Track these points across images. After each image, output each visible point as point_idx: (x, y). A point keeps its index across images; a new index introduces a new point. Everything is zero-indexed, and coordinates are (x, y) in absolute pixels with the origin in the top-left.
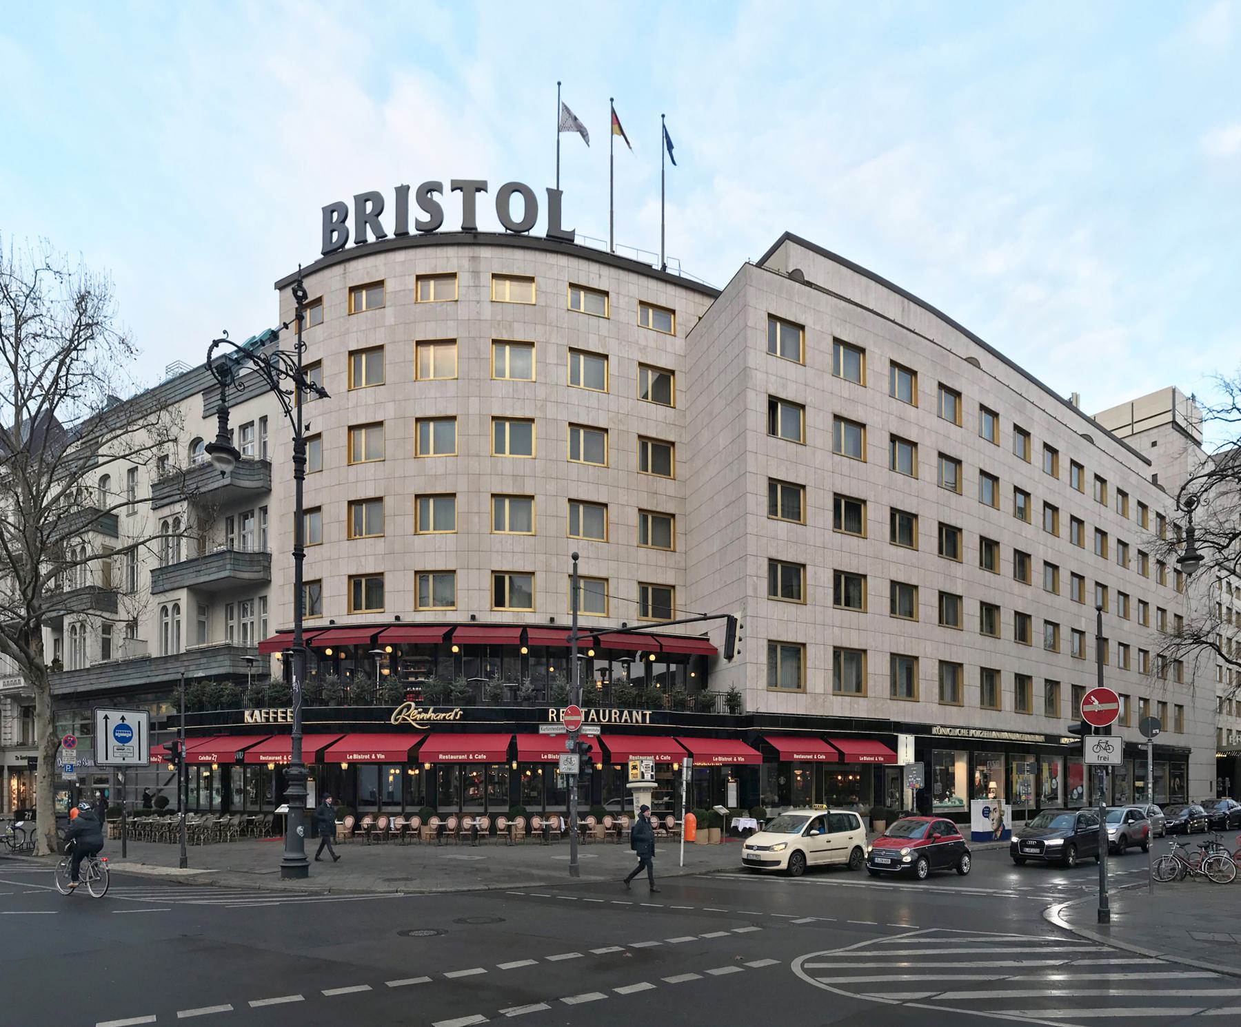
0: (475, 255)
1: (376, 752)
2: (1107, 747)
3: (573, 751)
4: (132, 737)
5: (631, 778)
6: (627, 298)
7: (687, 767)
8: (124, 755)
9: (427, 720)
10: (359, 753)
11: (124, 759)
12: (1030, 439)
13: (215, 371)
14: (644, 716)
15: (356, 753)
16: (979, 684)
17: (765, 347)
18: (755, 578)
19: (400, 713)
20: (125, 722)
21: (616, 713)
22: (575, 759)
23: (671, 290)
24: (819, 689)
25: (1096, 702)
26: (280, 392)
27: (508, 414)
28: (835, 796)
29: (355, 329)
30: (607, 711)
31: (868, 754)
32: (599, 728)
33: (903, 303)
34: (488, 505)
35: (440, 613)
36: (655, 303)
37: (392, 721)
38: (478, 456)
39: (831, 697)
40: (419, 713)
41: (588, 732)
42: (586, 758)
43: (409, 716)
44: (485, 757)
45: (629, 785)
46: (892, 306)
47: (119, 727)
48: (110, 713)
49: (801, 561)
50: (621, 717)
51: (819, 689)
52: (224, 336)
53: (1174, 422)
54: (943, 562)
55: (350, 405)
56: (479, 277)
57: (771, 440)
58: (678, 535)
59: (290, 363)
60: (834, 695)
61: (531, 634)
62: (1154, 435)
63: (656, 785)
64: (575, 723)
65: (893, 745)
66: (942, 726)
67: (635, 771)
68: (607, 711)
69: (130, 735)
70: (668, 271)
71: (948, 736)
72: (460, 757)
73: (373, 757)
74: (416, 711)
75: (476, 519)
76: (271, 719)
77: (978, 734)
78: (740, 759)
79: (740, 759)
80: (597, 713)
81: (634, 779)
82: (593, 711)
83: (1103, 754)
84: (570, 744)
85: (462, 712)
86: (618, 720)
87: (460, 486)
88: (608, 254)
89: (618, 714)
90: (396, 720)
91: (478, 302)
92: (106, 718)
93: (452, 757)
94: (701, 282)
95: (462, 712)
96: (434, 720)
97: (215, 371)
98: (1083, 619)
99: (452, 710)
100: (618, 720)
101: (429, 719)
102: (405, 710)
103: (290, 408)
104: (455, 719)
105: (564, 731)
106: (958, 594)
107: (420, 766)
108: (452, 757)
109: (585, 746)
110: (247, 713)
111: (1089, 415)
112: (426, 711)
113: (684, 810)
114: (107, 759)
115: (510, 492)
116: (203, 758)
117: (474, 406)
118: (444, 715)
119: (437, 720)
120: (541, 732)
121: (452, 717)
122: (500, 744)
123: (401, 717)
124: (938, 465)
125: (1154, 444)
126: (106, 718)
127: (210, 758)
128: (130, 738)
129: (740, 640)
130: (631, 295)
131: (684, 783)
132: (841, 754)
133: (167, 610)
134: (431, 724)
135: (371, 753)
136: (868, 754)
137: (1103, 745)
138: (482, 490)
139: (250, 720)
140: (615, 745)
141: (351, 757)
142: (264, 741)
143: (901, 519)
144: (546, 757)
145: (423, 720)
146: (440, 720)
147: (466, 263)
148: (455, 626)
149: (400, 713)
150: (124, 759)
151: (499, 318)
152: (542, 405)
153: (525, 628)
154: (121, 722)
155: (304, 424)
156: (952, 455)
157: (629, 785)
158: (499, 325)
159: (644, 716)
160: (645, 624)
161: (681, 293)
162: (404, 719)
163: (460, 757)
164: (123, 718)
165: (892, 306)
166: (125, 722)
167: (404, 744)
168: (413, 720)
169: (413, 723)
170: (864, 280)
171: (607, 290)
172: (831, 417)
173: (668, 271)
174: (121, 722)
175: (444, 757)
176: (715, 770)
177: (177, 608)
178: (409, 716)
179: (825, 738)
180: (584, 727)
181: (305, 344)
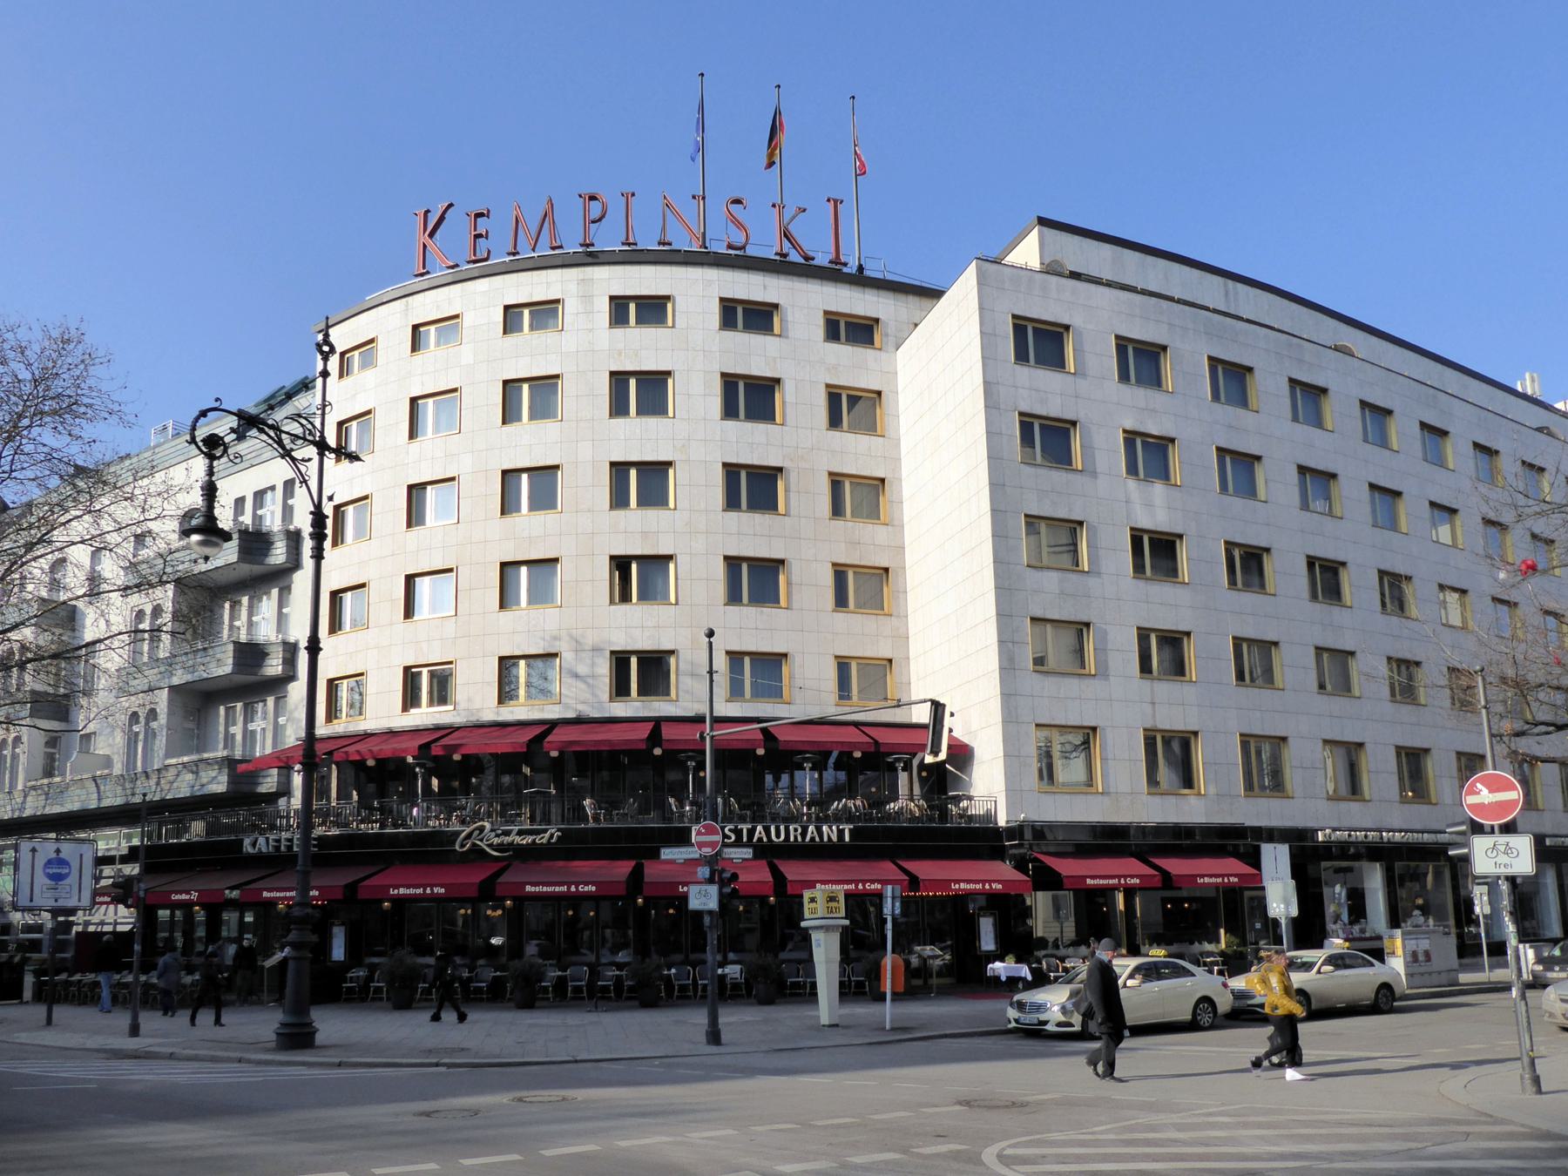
1: (1229, 876)
2: (1508, 850)
3: (711, 881)
4: (70, 873)
5: (807, 915)
7: (893, 898)
8: (57, 895)
10: (968, 882)
11: (56, 901)
13: (200, 444)
14: (841, 833)
15: (964, 881)
16: (1395, 769)
18: (1010, 645)
20: (61, 855)
21: (796, 830)
22: (713, 890)
25: (1485, 791)
26: (294, 459)
30: (782, 828)
31: (1213, 873)
32: (751, 850)
33: (1225, 285)
37: (457, 848)
40: (498, 836)
41: (732, 856)
42: (727, 890)
44: (594, 889)
45: (803, 924)
46: (1210, 290)
47: (49, 863)
48: (36, 843)
50: (804, 834)
52: (217, 405)
54: (1320, 610)
59: (310, 427)
60: (1149, 794)
61: (668, 732)
63: (847, 922)
64: (712, 844)
65: (1254, 859)
67: (813, 905)
68: (782, 828)
69: (67, 871)
72: (557, 889)
73: (1226, 880)
74: (493, 834)
76: (283, 848)
77: (1398, 837)
78: (1232, 879)
79: (1232, 879)
80: (767, 830)
81: (812, 916)
82: (759, 828)
83: (703, 899)
84: (703, 872)
85: (559, 834)
86: (800, 839)
89: (800, 830)
90: (462, 846)
91: (591, 330)
92: (34, 850)
93: (545, 889)
95: (559, 834)
97: (200, 444)
98: (1072, 371)
99: (545, 831)
100: (800, 839)
103: (307, 478)
105: (697, 856)
107: (498, 902)
108: (545, 889)
109: (727, 875)
110: (247, 842)
114: (79, 901)
116: (178, 897)
120: (663, 857)
122: (622, 869)
124: (1300, 482)
126: (34, 850)
127: (187, 897)
128: (67, 875)
129: (952, 715)
131: (889, 919)
132: (1166, 875)
133: (139, 716)
134: (514, 850)
135: (1223, 876)
136: (1213, 873)
137: (1502, 848)
139: (250, 850)
140: (793, 871)
141: (396, 891)
142: (277, 873)
144: (396, 891)
145: (502, 844)
148: (552, 725)
149: (469, 836)
150: (56, 901)
152: (683, 446)
153: (658, 722)
154: (54, 855)
155: (326, 494)
156: (1321, 467)
157: (803, 924)
160: (847, 709)
163: (557, 889)
164: (58, 851)
166: (61, 855)
167: (474, 877)
170: (1162, 263)
174: (54, 855)
175: (533, 889)
176: (961, 900)
177: (153, 714)
178: (481, 840)
179: (1142, 855)
180: (726, 850)
181: (330, 404)
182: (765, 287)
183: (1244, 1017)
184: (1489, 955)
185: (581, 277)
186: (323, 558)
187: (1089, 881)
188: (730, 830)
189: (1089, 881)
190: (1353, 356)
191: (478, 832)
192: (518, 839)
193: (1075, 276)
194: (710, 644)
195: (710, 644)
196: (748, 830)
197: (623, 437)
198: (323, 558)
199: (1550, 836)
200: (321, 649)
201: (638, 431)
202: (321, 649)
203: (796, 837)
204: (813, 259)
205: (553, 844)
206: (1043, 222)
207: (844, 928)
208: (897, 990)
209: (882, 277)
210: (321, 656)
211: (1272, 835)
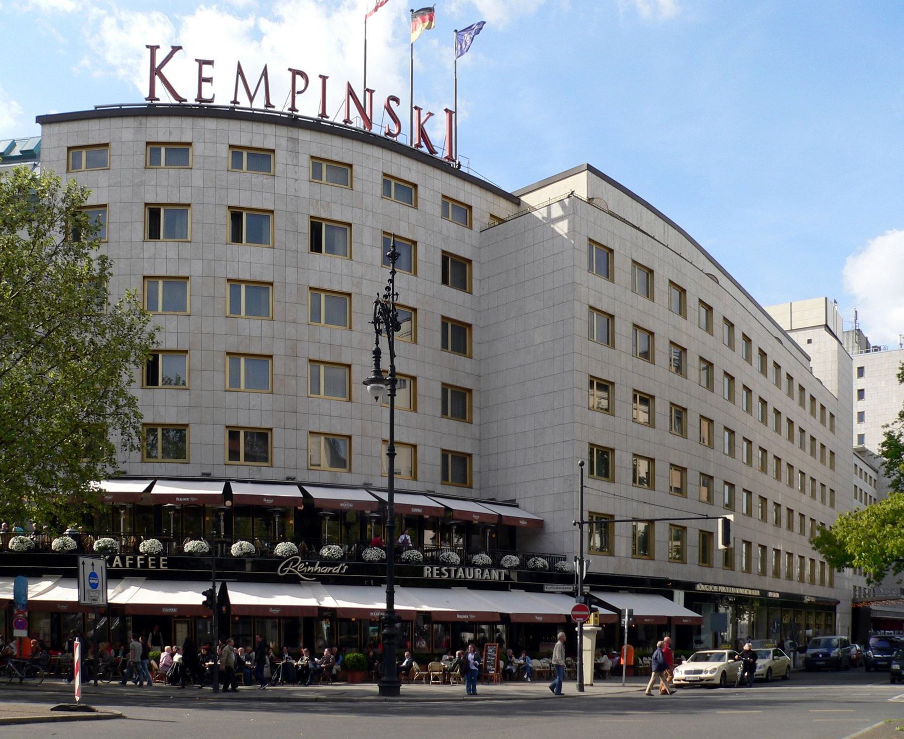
0: (294, 137)
6: (432, 192)
9: (314, 572)
12: (751, 344)
17: (586, 267)
19: (287, 565)
23: (468, 187)
24: (623, 554)
27: (326, 286)
28: (531, 637)
29: (153, 183)
34: (305, 370)
35: (255, 468)
36: (455, 198)
38: (295, 322)
39: (631, 559)
43: (296, 568)
49: (611, 446)
50: (482, 574)
51: (623, 554)
53: (826, 326)
55: (146, 255)
56: (297, 157)
57: (444, 287)
58: (474, 409)
60: (632, 558)
62: (809, 334)
66: (703, 584)
69: (96, 582)
70: (462, 169)
71: (706, 591)
74: (303, 564)
75: (293, 382)
86: (430, 575)
87: (278, 349)
88: (408, 147)
90: (282, 571)
91: (296, 180)
94: (483, 179)
96: (320, 573)
101: (316, 572)
102: (292, 563)
104: (340, 573)
106: (683, 466)
111: (509, 191)
112: (313, 565)
113: (130, 633)
115: (327, 359)
117: (291, 275)
118: (330, 569)
119: (323, 573)
121: (338, 571)
123: (288, 569)
125: (809, 341)
130: (436, 189)
138: (299, 355)
143: (676, 410)
146: (326, 573)
147: (283, 142)
151: (318, 197)
152: (358, 283)
158: (317, 204)
159: (500, 573)
161: (476, 190)
162: (290, 571)
165: (673, 238)
168: (300, 572)
169: (300, 575)
171: (415, 182)
172: (631, 326)
173: (462, 169)
178: (296, 568)
182: (410, 170)
183: (822, 669)
184: (626, 676)
185: (290, 135)
186: (395, 395)
187: (458, 616)
188: (445, 570)
189: (458, 616)
190: (718, 283)
191: (292, 563)
192: (320, 569)
193: (612, 214)
194: (582, 469)
195: (582, 469)
196: (455, 570)
197: (318, 269)
198: (395, 395)
199: (771, 592)
200: (396, 454)
201: (329, 266)
202: (396, 454)
203: (478, 576)
204: (437, 153)
205: (343, 574)
206: (590, 168)
207: (598, 631)
208: (629, 664)
209: (467, 172)
210: (396, 459)
211: (678, 585)
